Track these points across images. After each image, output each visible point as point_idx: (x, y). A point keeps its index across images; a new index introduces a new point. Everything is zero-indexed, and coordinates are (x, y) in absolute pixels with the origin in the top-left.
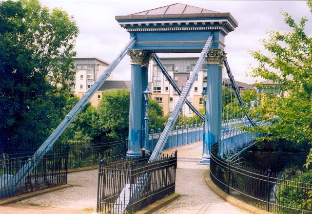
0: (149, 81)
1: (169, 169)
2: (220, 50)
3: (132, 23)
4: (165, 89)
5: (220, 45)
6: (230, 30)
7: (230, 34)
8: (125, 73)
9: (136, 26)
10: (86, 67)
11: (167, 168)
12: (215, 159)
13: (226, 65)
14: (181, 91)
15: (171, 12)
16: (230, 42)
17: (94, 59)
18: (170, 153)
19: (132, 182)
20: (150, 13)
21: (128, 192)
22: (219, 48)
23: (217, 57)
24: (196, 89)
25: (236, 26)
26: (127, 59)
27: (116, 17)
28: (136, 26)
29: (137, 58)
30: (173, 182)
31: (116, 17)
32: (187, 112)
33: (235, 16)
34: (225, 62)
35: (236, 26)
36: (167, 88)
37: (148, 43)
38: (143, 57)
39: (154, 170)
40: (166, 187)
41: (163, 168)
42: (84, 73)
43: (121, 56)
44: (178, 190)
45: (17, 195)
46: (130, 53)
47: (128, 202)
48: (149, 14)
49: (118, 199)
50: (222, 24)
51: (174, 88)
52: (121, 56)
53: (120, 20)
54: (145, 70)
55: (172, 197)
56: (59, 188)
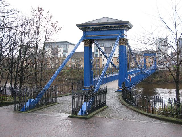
0: (93, 52)
1: (103, 95)
2: (125, 38)
3: (84, 27)
4: (100, 55)
5: (125, 36)
6: (129, 28)
7: (130, 30)
8: (81, 48)
9: (84, 27)
10: (62, 46)
11: (102, 94)
12: (124, 89)
13: (128, 45)
14: (107, 55)
15: (103, 21)
16: (129, 34)
17: (66, 42)
18: (103, 87)
19: (87, 102)
20: (92, 22)
21: (85, 105)
22: (125, 37)
23: (124, 42)
24: (115, 55)
25: (132, 26)
26: (82, 44)
27: (77, 24)
28: (84, 27)
29: (87, 43)
30: (105, 101)
31: (77, 24)
32: (110, 66)
33: (131, 22)
34: (127, 44)
35: (132, 26)
36: (101, 55)
37: (91, 35)
38: (88, 41)
39: (97, 96)
40: (102, 103)
41: (100, 95)
42: (62, 49)
43: (79, 43)
44: (107, 104)
45: (36, 108)
46: (84, 41)
47: (85, 109)
48: (92, 23)
49: (81, 109)
50: (125, 26)
51: (104, 56)
52: (79, 43)
53: (79, 26)
54: (91, 48)
55: (105, 107)
56: (53, 104)
